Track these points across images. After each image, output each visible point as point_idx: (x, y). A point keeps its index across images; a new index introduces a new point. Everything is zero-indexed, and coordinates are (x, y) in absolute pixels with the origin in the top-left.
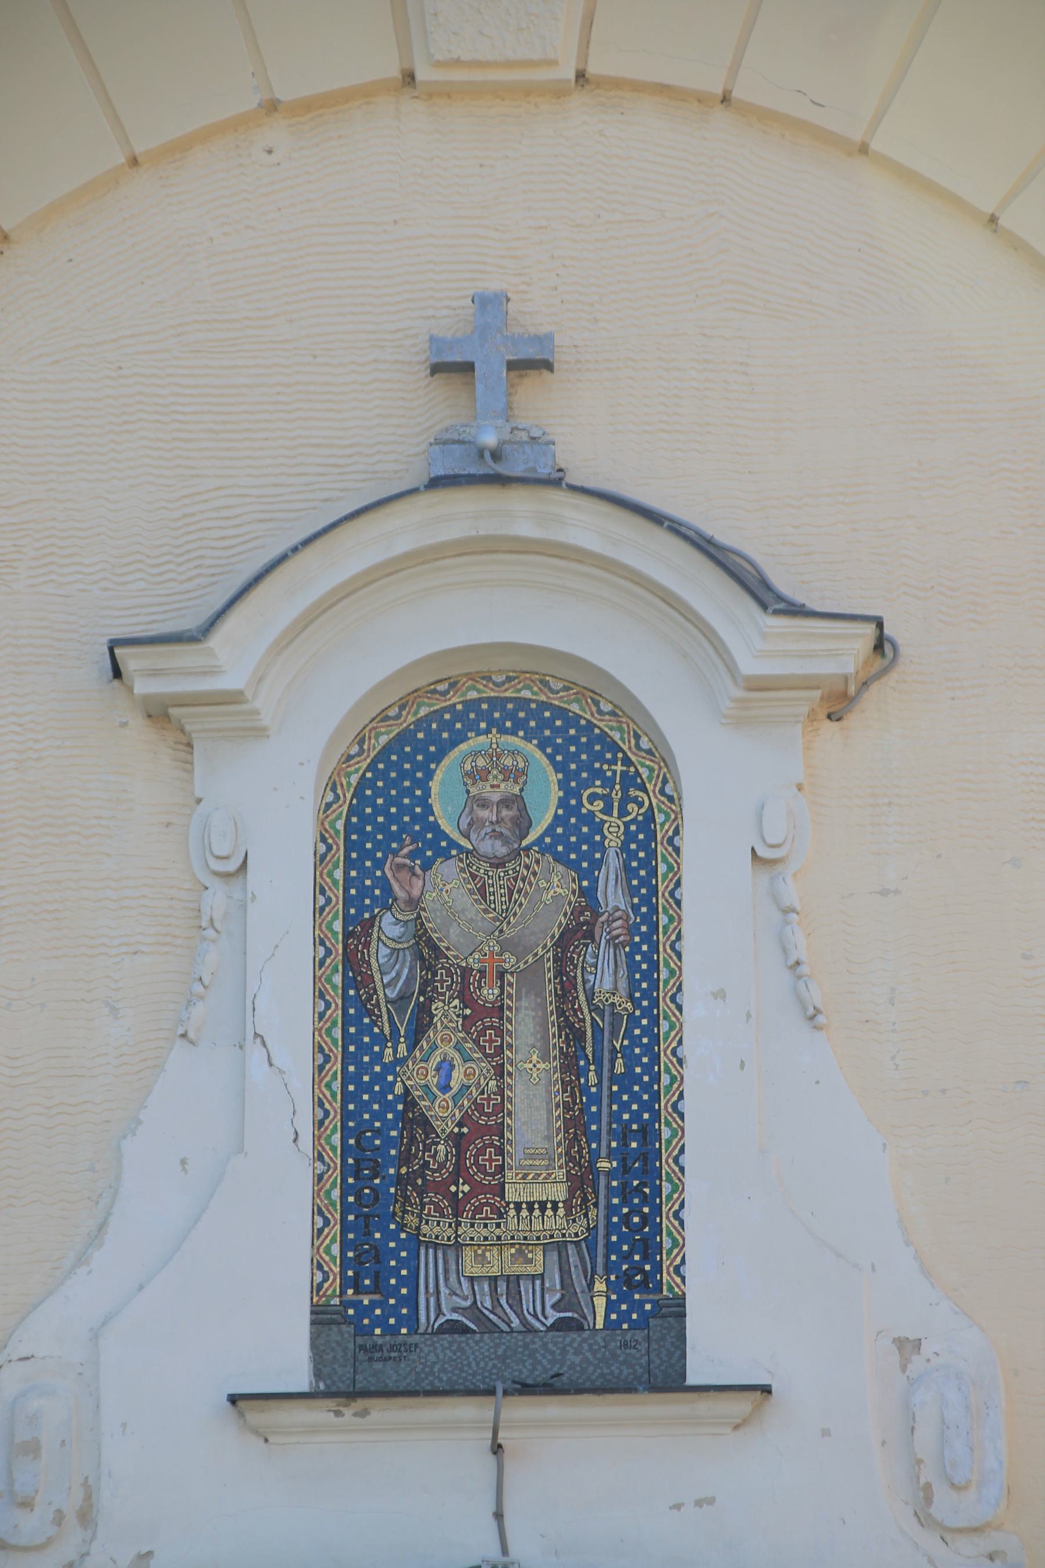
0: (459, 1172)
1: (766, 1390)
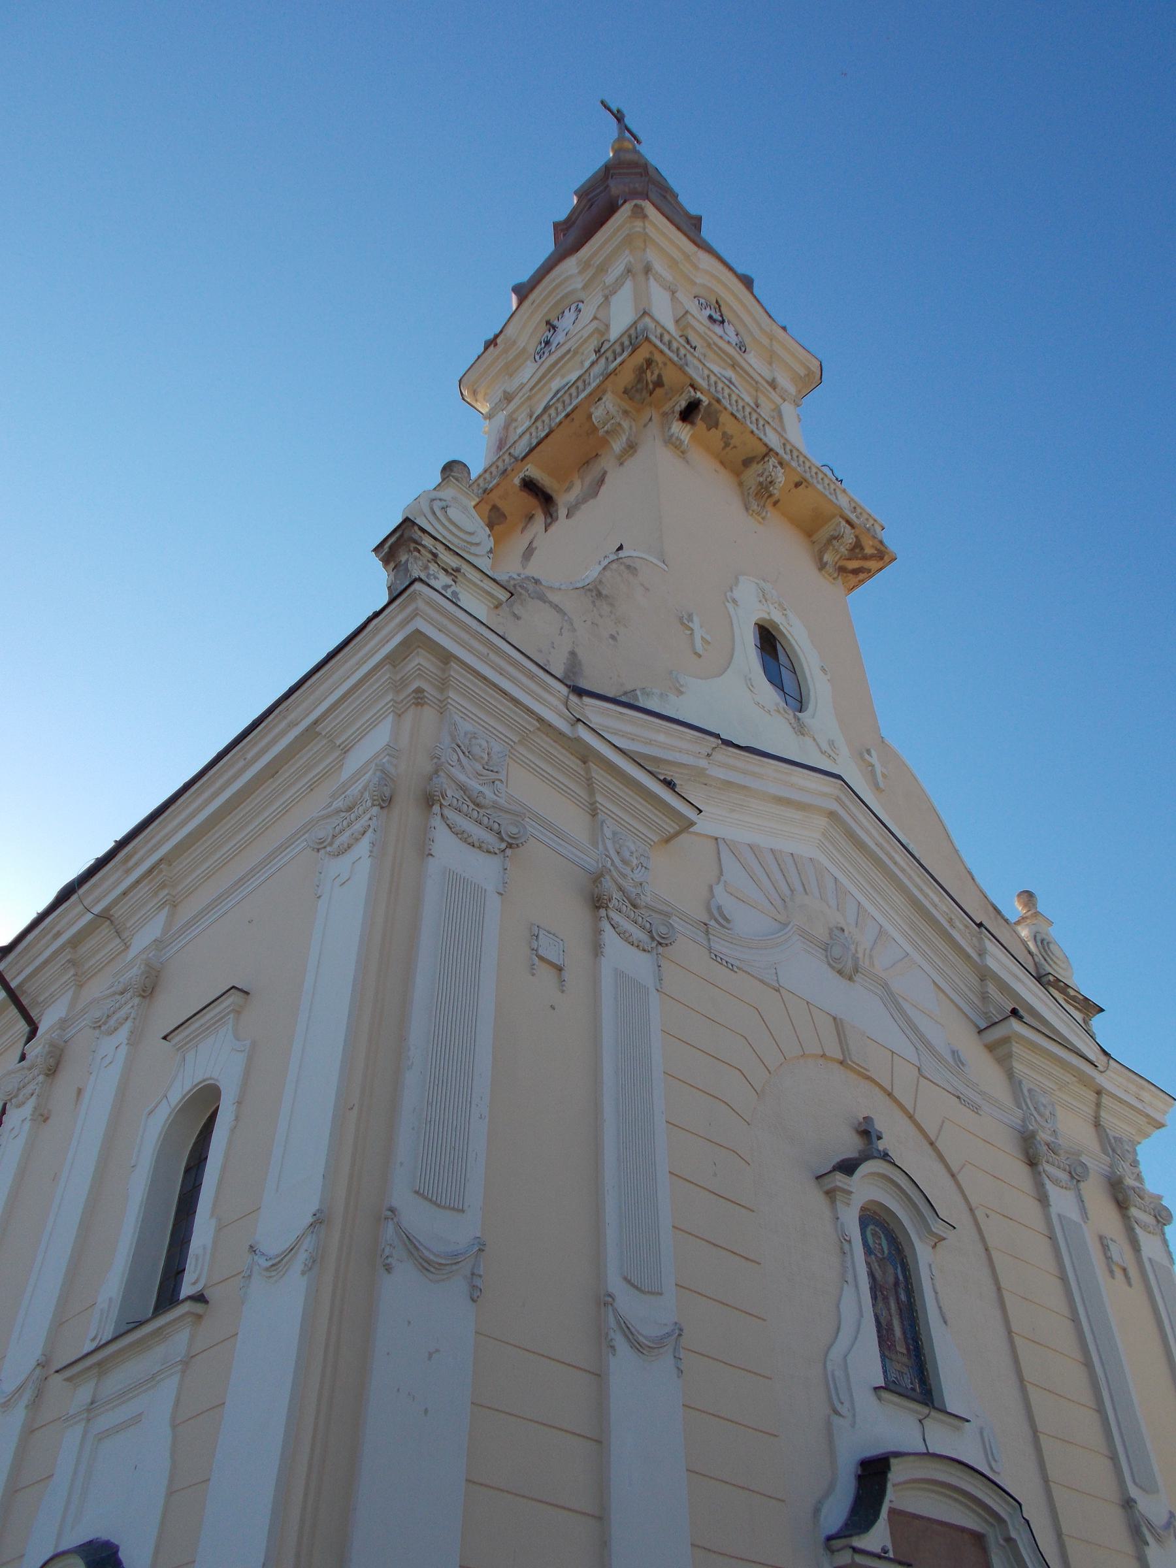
0: (888, 1339)
1: (417, 1192)
